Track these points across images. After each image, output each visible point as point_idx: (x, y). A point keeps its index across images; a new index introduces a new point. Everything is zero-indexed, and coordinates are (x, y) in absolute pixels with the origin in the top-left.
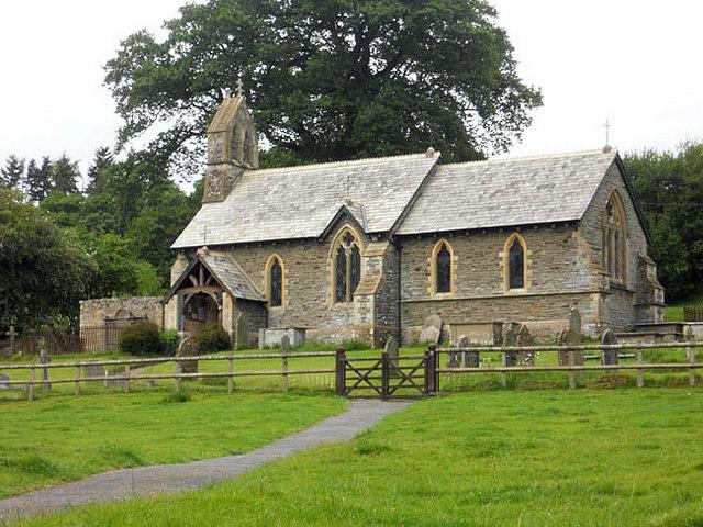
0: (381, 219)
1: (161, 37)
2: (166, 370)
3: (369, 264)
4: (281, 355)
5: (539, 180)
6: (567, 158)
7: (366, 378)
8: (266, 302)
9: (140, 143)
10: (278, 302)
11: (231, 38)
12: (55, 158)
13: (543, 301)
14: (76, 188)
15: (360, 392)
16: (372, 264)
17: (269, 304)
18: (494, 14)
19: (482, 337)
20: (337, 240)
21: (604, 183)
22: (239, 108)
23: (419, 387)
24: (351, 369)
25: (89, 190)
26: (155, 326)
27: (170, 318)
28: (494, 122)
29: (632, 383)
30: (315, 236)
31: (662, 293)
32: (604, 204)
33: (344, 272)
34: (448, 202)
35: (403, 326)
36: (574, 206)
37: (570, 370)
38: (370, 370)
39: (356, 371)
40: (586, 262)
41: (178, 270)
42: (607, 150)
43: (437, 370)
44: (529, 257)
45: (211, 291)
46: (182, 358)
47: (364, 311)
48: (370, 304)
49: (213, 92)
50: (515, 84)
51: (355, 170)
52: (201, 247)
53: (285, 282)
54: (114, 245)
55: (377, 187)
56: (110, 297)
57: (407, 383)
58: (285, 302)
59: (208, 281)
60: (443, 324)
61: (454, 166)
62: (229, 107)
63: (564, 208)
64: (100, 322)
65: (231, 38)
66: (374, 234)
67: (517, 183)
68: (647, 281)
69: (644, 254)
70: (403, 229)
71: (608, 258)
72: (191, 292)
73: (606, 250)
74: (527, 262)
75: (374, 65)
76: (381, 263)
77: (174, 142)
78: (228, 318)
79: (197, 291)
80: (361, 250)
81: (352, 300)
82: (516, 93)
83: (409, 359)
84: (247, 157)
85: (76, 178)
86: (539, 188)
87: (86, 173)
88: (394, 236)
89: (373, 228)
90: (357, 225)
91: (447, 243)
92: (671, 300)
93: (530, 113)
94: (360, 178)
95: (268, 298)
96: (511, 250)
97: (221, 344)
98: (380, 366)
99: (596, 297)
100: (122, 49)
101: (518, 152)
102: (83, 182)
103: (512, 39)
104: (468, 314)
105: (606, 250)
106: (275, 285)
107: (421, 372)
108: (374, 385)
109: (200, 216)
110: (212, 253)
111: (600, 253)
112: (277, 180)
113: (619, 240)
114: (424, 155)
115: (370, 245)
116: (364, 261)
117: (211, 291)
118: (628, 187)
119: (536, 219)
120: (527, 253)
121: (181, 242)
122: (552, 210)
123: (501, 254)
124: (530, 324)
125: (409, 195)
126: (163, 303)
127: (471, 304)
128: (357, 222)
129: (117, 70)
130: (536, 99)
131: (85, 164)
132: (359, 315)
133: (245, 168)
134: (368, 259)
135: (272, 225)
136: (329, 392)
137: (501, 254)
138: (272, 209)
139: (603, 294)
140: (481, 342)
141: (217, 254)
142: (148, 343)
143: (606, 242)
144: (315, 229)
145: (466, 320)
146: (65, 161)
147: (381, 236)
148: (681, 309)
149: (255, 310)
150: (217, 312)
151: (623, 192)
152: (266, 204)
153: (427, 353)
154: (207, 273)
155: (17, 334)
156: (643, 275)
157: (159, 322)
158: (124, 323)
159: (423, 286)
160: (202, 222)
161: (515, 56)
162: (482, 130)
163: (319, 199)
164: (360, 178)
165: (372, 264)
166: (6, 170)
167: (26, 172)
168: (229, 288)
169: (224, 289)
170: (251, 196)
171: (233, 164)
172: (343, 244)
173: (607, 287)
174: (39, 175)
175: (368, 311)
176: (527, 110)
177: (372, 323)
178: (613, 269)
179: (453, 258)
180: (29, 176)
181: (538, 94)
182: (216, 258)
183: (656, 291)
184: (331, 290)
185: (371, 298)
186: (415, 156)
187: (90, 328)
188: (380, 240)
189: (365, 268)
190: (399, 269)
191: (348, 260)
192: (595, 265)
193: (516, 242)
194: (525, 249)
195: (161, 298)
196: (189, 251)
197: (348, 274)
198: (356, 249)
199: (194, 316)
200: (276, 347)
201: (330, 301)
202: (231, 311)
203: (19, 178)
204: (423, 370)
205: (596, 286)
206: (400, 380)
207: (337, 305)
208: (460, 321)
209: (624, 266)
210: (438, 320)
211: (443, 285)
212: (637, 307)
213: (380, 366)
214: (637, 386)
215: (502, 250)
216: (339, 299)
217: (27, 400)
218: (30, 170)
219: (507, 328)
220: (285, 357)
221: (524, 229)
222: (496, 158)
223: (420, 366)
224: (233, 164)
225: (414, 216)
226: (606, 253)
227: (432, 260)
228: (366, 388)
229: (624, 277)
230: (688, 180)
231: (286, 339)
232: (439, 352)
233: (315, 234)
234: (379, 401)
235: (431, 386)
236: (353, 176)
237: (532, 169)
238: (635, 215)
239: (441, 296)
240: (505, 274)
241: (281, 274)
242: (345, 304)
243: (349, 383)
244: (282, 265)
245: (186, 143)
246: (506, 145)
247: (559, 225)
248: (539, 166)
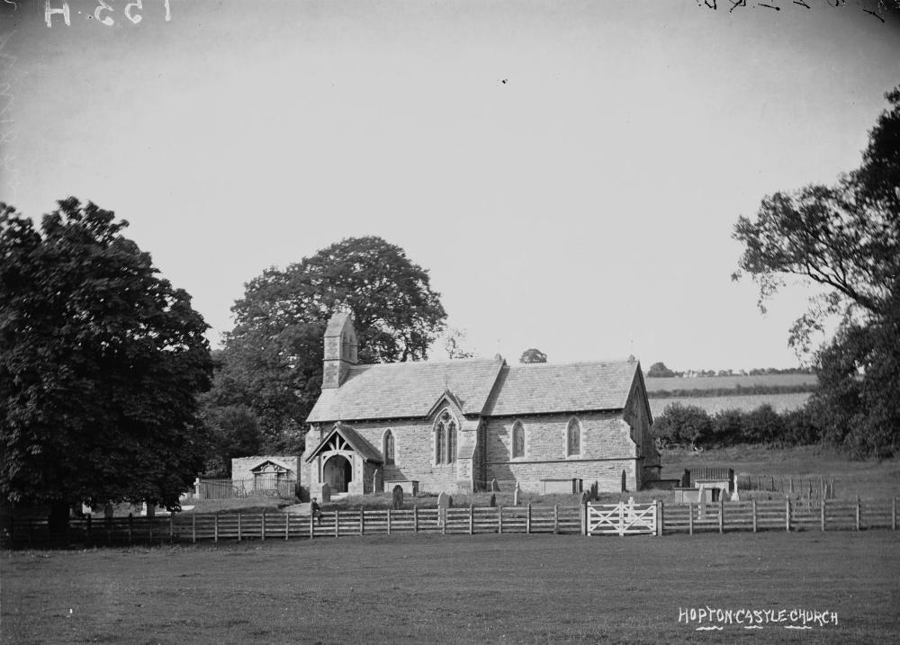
20: (438, 418)
52: (336, 421)
59: (343, 446)
165: (467, 438)
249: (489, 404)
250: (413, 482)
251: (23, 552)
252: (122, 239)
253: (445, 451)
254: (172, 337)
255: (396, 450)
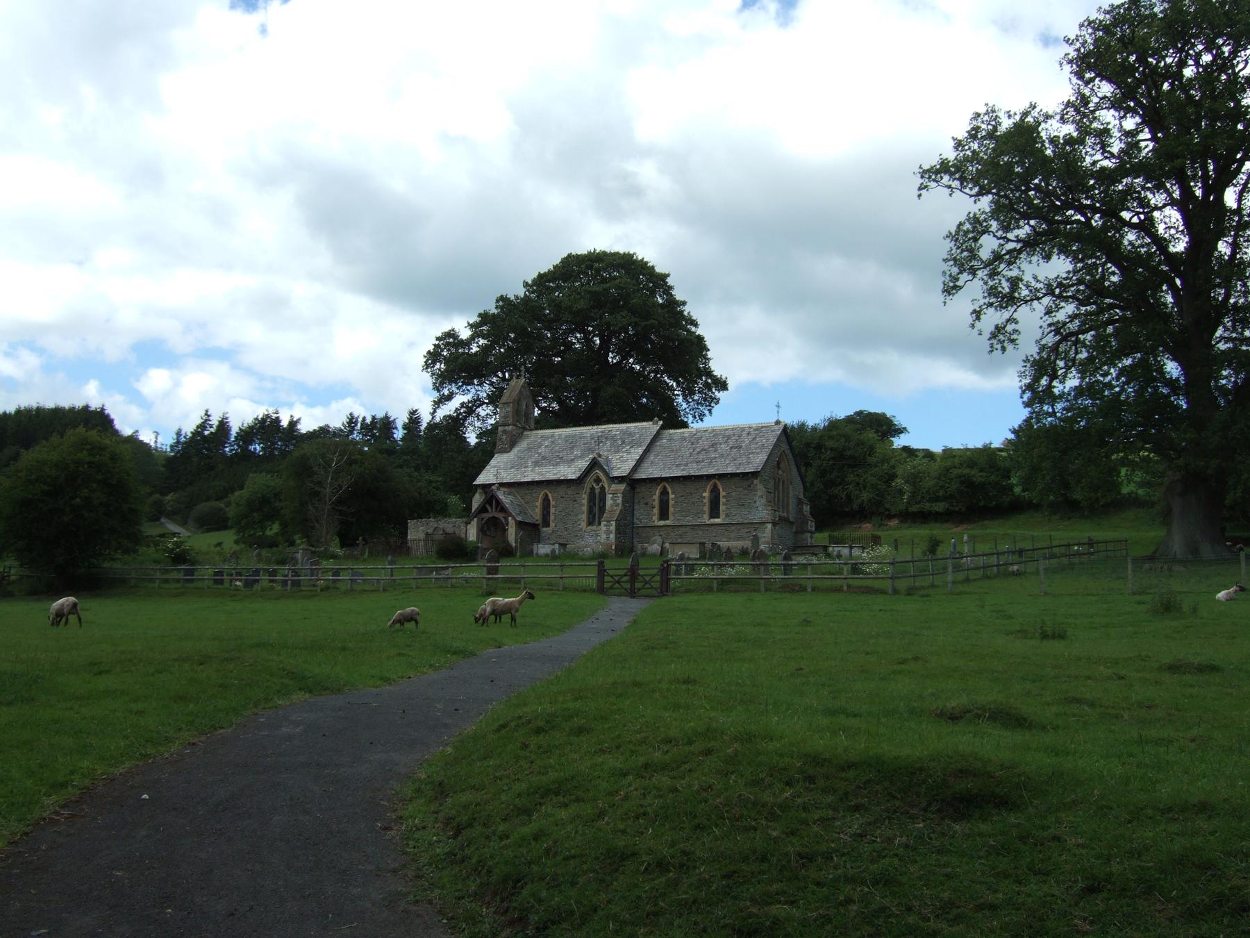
0: (622, 464)
1: (465, 334)
2: (474, 572)
3: (612, 499)
4: (559, 564)
5: (731, 443)
6: (750, 428)
7: (618, 582)
8: (539, 525)
9: (448, 409)
10: (546, 524)
11: (512, 335)
12: (380, 415)
13: (733, 528)
14: (394, 438)
15: (643, 592)
16: (614, 500)
17: (541, 525)
18: (696, 325)
19: (693, 553)
20: (590, 481)
21: (776, 445)
22: (522, 387)
23: (656, 589)
24: (608, 575)
25: (402, 439)
26: (460, 538)
27: (472, 533)
28: (693, 400)
29: (803, 589)
30: (574, 478)
31: (813, 524)
32: (775, 461)
33: (595, 504)
34: (667, 457)
35: (635, 544)
36: (756, 462)
37: (762, 579)
38: (622, 576)
39: (612, 576)
40: (763, 501)
41: (477, 500)
42: (778, 422)
43: (669, 577)
44: (724, 497)
45: (500, 516)
46: (489, 564)
47: (608, 532)
48: (613, 528)
49: (500, 374)
50: (709, 373)
51: (603, 432)
52: (494, 484)
53: (552, 510)
54: (431, 482)
55: (618, 444)
56: (429, 518)
57: (647, 586)
58: (552, 525)
59: (499, 509)
60: (663, 543)
61: (672, 431)
62: (514, 386)
63: (749, 463)
64: (422, 536)
65: (512, 335)
66: (617, 478)
67: (715, 444)
68: (803, 515)
69: (801, 496)
70: (637, 475)
71: (777, 499)
72: (486, 516)
73: (776, 492)
74: (722, 500)
75: (612, 358)
76: (621, 498)
77: (470, 409)
78: (512, 534)
79: (491, 516)
80: (607, 488)
81: (600, 524)
82: (709, 381)
83: (649, 569)
84: (527, 421)
85: (394, 431)
86: (731, 448)
87: (401, 427)
88: (630, 480)
89: (616, 474)
90: (604, 471)
91: (667, 485)
92: (819, 528)
93: (718, 394)
94: (607, 438)
95: (540, 522)
96: (711, 492)
97: (507, 552)
98: (629, 574)
99: (769, 526)
100: (437, 342)
101: (710, 422)
102: (399, 434)
103: (708, 343)
104: (681, 536)
105: (776, 492)
106: (545, 512)
107: (658, 578)
108: (655, 586)
109: (493, 462)
110: (502, 489)
111: (772, 495)
112: (548, 438)
113: (785, 486)
114: (651, 423)
115: (613, 485)
116: (609, 497)
117: (500, 516)
118: (791, 448)
119: (730, 470)
120: (722, 493)
121: (481, 479)
122: (740, 464)
123: (705, 494)
124: (724, 544)
125: (640, 451)
126: (467, 523)
127: (684, 529)
128: (604, 469)
129: (433, 357)
130: (722, 385)
131: (401, 418)
132: (605, 535)
133: (525, 429)
134: (611, 496)
135: (544, 470)
136: (593, 591)
137: (705, 494)
138: (544, 458)
139: (774, 524)
140: (691, 556)
141: (505, 490)
142: (454, 550)
143: (776, 487)
144: (574, 473)
145: (679, 540)
146: (387, 418)
147: (620, 479)
148: (826, 534)
149: (531, 531)
150: (505, 531)
151: (788, 452)
152: (539, 454)
153: (662, 565)
154: (498, 502)
155: (364, 542)
156: (800, 511)
157: (463, 536)
158: (439, 536)
159: (650, 516)
160: (494, 467)
161: (710, 354)
162: (684, 405)
163: (577, 452)
164: (607, 438)
165: (614, 500)
166: (345, 423)
167: (359, 425)
168: (513, 514)
169: (510, 515)
170: (529, 449)
171: (517, 426)
172: (594, 485)
173: (777, 519)
174: (368, 428)
175: (612, 532)
176: (717, 393)
177: (614, 541)
178: (781, 507)
179: (672, 496)
180: (361, 428)
181: (725, 382)
182: (504, 492)
183: (810, 522)
184: (584, 517)
185: (613, 523)
186: (645, 424)
187: (415, 540)
188: (620, 482)
189: (609, 502)
190: (633, 503)
191: (597, 495)
192: (769, 504)
193: (715, 486)
194: (721, 490)
195: (465, 519)
196: (486, 487)
197: (597, 506)
198: (603, 488)
199: (488, 533)
200: (547, 555)
201: (584, 524)
202: (514, 530)
203: (354, 430)
204: (659, 577)
205: (769, 518)
206: (642, 584)
207: (590, 527)
208: (674, 541)
209: (788, 505)
210: (659, 540)
211: (664, 514)
212: (796, 533)
213: (629, 574)
214: (807, 591)
215: (705, 491)
216: (590, 523)
217: (379, 591)
218: (362, 424)
219: (708, 546)
220: (562, 566)
221: (721, 477)
222: (695, 426)
223: (625, 575)
224: (517, 426)
225: (645, 465)
226: (776, 495)
227: (656, 497)
228: (619, 588)
229: (788, 512)
230: (830, 444)
231: (553, 551)
232: (670, 565)
233: (574, 477)
234: (628, 598)
235: (665, 589)
236: (602, 436)
237: (715, 433)
238: (796, 469)
239: (662, 523)
240: (706, 508)
241: (550, 505)
242: (594, 527)
243: (607, 585)
244: (550, 498)
245: (479, 410)
246: (702, 416)
247: (745, 474)
248: (731, 432)
249: (635, 468)
250: (700, 543)
251: (696, 598)
252: (80, 425)
253: (596, 515)
254: (294, 439)
255: (670, 505)
